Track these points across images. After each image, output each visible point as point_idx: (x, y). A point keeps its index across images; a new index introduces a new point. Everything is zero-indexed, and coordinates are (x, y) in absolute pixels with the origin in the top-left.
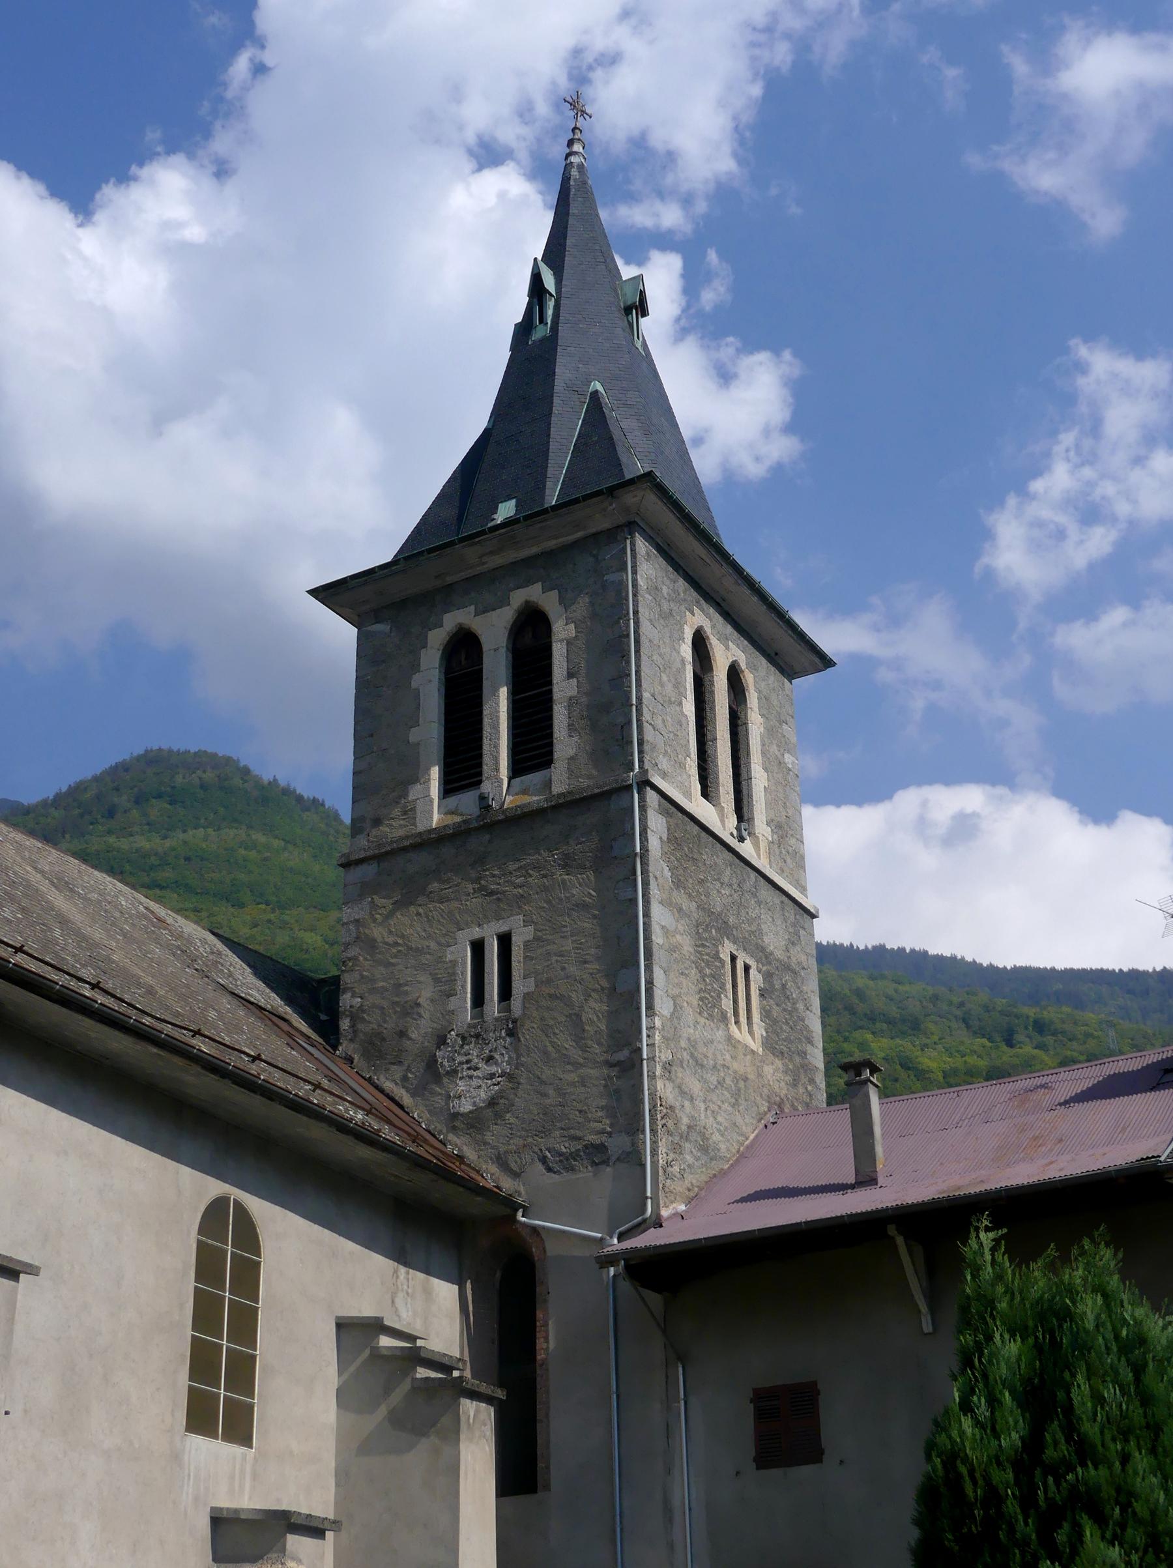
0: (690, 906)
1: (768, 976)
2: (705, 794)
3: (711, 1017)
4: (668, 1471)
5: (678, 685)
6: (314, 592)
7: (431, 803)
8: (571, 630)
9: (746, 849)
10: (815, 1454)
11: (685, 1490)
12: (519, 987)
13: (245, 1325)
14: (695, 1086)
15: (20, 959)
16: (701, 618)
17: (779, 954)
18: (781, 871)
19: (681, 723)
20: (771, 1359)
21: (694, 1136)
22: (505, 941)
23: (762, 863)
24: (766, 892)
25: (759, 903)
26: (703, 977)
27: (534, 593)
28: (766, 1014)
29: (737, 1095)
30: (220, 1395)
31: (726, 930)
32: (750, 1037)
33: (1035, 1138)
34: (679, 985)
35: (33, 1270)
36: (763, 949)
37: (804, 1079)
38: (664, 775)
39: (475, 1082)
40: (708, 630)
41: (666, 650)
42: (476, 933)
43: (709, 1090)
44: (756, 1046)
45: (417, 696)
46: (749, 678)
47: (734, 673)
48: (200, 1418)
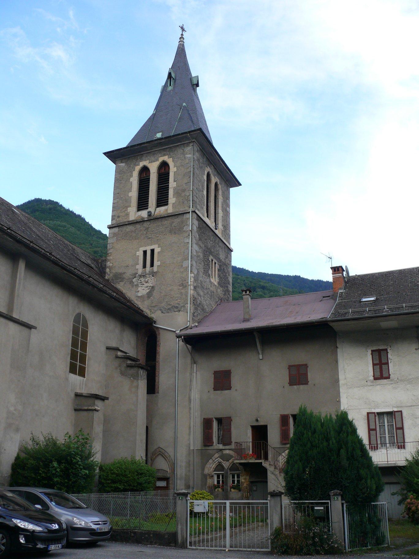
0: (203, 246)
1: (220, 266)
2: (207, 217)
3: (206, 275)
4: (191, 390)
5: (203, 186)
6: (105, 154)
7: (133, 214)
8: (175, 169)
9: (217, 232)
10: (229, 388)
11: (195, 395)
12: (156, 263)
13: (84, 346)
14: (202, 293)
15: (31, 244)
16: (208, 169)
17: (223, 260)
18: (225, 239)
19: (203, 197)
20: (220, 363)
21: (200, 306)
22: (153, 251)
23: (220, 235)
24: (221, 244)
25: (219, 246)
26: (205, 264)
27: (166, 158)
28: (219, 276)
29: (211, 296)
30: (78, 365)
31: (211, 253)
32: (215, 280)
33: (291, 312)
34: (199, 266)
35: (35, 328)
36: (219, 259)
37: (227, 294)
38: (198, 210)
39: (143, 288)
40: (211, 172)
41: (200, 177)
42: (144, 249)
43: (205, 295)
44: (216, 284)
45: (132, 184)
46: (220, 186)
47: (216, 184)
48: (73, 370)
